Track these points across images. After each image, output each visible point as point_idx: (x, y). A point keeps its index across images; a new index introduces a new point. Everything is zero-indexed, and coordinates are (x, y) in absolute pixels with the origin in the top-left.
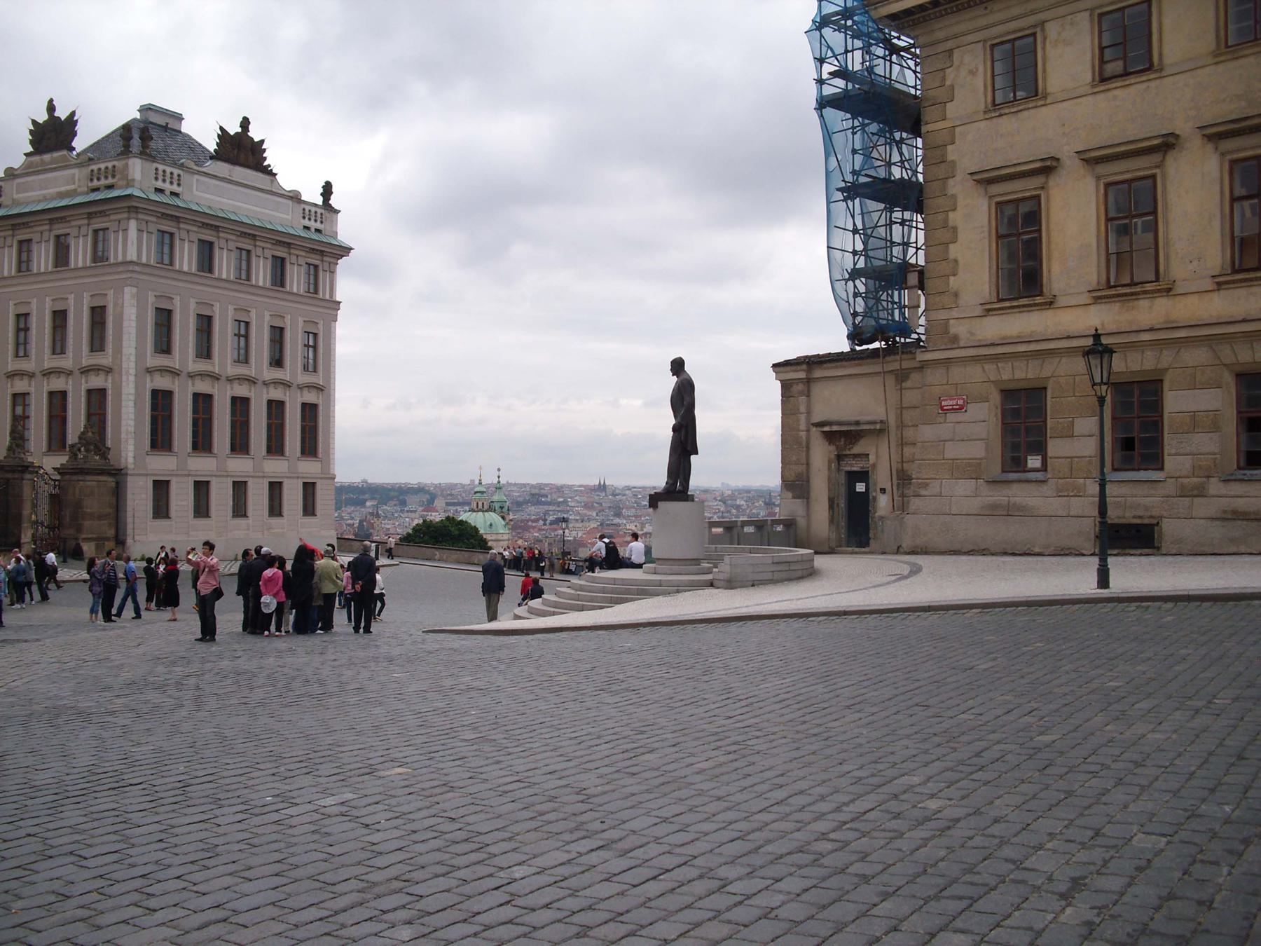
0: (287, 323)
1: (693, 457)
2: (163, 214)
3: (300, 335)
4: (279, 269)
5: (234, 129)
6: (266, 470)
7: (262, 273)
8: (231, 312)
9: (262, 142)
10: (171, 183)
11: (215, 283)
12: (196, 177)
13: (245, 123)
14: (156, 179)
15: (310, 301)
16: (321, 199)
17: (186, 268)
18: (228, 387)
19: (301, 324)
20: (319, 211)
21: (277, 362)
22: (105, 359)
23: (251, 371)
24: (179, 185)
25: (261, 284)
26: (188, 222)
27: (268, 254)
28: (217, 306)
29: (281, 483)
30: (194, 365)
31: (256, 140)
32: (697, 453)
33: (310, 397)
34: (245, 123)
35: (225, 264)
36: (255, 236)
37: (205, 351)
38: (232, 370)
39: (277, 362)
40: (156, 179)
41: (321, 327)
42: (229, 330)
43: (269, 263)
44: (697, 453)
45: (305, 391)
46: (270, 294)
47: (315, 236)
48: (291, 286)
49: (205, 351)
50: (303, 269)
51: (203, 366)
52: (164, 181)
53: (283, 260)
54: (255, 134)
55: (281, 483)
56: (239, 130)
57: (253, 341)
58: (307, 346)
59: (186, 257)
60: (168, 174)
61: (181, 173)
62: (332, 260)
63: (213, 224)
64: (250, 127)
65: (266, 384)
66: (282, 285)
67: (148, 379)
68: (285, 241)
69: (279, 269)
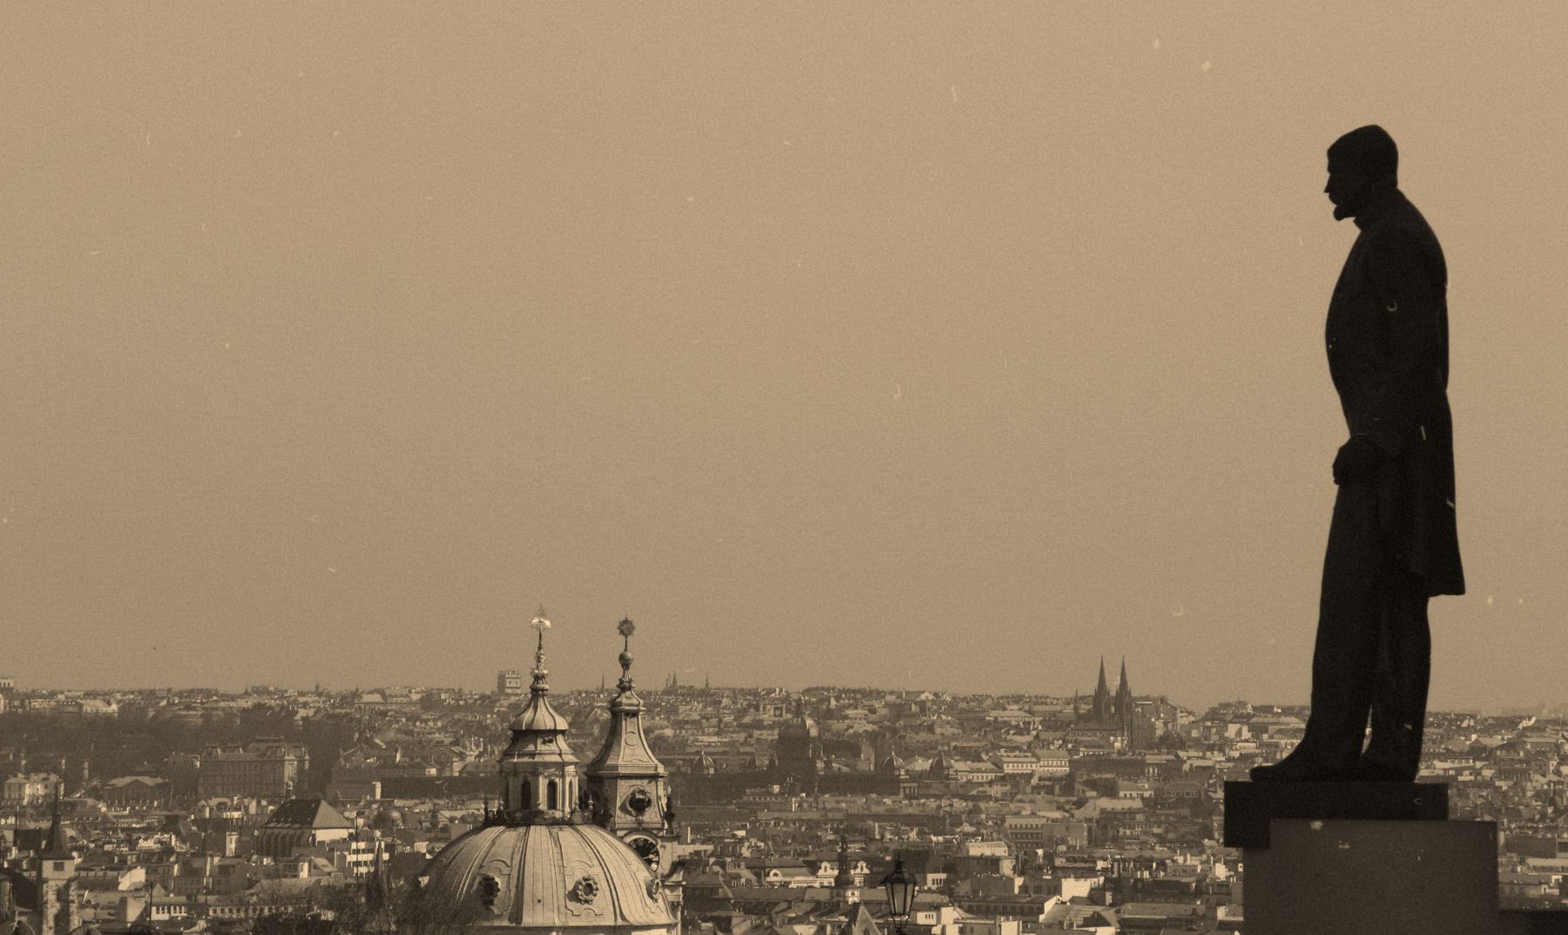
1: (1439, 608)
32: (1455, 585)
44: (1455, 585)
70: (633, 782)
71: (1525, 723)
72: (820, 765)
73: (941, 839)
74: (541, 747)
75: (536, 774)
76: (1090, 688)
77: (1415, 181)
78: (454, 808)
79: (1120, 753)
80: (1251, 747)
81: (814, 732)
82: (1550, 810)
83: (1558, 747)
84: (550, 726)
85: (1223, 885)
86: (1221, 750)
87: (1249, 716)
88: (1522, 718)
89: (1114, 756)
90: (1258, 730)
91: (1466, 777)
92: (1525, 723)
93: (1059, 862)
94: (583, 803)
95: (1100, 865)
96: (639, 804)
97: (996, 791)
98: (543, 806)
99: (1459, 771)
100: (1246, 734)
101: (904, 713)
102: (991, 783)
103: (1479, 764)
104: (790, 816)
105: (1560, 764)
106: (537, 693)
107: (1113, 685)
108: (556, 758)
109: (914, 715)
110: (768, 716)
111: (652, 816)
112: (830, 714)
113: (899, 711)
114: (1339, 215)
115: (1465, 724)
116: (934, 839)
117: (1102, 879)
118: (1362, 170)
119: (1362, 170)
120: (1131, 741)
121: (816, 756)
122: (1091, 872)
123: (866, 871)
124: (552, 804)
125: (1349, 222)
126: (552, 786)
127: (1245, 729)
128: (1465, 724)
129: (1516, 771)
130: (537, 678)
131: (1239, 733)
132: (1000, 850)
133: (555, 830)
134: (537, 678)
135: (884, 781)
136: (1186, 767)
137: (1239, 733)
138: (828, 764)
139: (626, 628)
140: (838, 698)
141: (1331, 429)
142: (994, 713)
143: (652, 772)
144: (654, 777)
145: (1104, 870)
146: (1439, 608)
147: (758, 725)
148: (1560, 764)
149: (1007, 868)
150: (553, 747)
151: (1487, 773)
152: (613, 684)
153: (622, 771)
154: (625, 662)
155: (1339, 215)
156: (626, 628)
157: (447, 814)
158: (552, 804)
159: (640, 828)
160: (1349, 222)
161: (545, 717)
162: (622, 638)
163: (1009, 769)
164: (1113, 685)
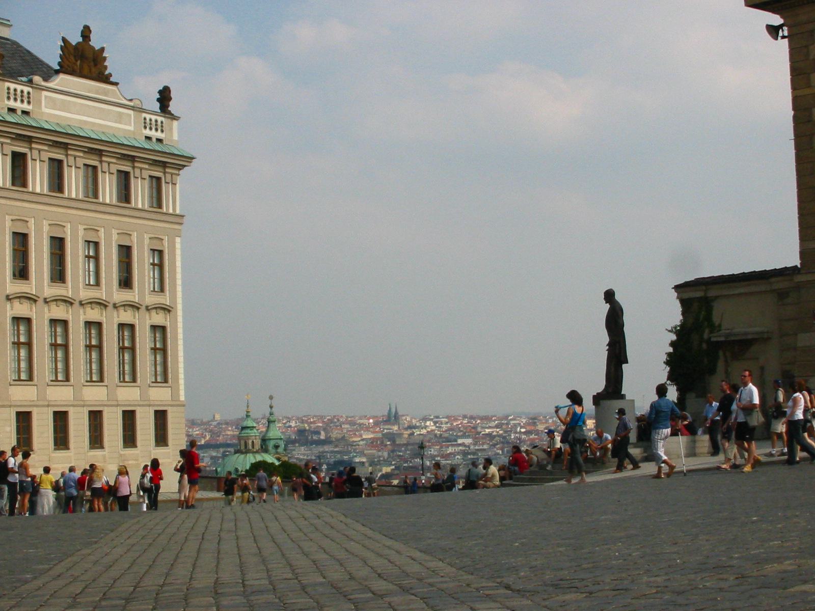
0: (31, 230)
1: (624, 366)
2: (57, 142)
3: (81, 244)
4: (124, 180)
5: (75, 38)
6: (120, 398)
7: (108, 189)
8: (81, 233)
9: (102, 49)
10: (22, 101)
11: (65, 203)
12: (45, 93)
13: (86, 33)
14: (9, 98)
15: (17, 195)
16: (158, 105)
17: (38, 190)
18: (81, 311)
19: (147, 241)
20: (154, 118)
21: (126, 283)
22: (165, 300)
23: (101, 294)
24: (29, 103)
25: (108, 201)
26: (78, 148)
27: (146, 174)
28: (32, 221)
29: (100, 412)
30: (51, 291)
31: (97, 48)
32: (627, 363)
33: (158, 319)
34: (86, 33)
35: (38, 176)
36: (134, 157)
37: (59, 275)
38: (85, 294)
39: (126, 283)
40: (9, 98)
41: (166, 244)
42: (146, 261)
43: (114, 177)
44: (627, 363)
45: (53, 306)
46: (46, 200)
47: (158, 147)
48: (136, 202)
49: (59, 275)
50: (147, 183)
51: (57, 290)
52: (151, 129)
53: (60, 162)
54: (96, 42)
55: (100, 412)
56: (81, 40)
57: (103, 262)
58: (88, 257)
59: (38, 176)
60: (19, 92)
61: (30, 90)
62: (176, 172)
63: (62, 140)
64: (92, 36)
65: (148, 309)
66: (96, 196)
67: (46, 309)
68: (129, 155)
69: (124, 180)
70: (274, 441)
71: (510, 418)
72: (310, 438)
73: (347, 457)
74: (250, 432)
75: (248, 439)
76: (386, 413)
77: (618, 297)
78: (203, 453)
79: (396, 431)
80: (434, 428)
81: (307, 428)
82: (518, 442)
83: (520, 424)
84: (252, 425)
85: (429, 467)
86: (425, 428)
87: (432, 419)
88: (509, 416)
89: (395, 432)
90: (435, 423)
91: (495, 433)
92: (510, 418)
93: (381, 462)
94: (262, 447)
95: (393, 463)
96: (277, 447)
97: (361, 443)
98: (251, 447)
99: (493, 432)
100: (432, 424)
101: (331, 423)
102: (359, 441)
103: (498, 430)
104: (302, 452)
105: (520, 428)
106: (248, 416)
107: (393, 411)
108: (254, 434)
109: (336, 422)
110: (293, 424)
111: (280, 450)
112: (311, 423)
113: (331, 421)
114: (606, 303)
115: (493, 419)
116: (345, 457)
117: (394, 467)
118: (609, 296)
119: (609, 296)
120: (399, 427)
121: (308, 435)
122: (391, 465)
123: (326, 467)
124: (253, 447)
125: (608, 304)
126: (253, 442)
127: (432, 422)
128: (493, 419)
129: (508, 431)
130: (248, 412)
131: (430, 424)
132: (364, 460)
133: (254, 454)
134: (248, 412)
135: (327, 442)
136: (415, 434)
137: (430, 424)
138: (312, 437)
139: (271, 398)
140: (313, 418)
141: (606, 339)
142: (359, 421)
143: (279, 438)
144: (281, 439)
145: (395, 464)
146: (624, 366)
147: (290, 427)
148: (520, 428)
149: (367, 465)
150: (253, 431)
151: (501, 432)
152: (268, 415)
153: (271, 438)
154: (271, 407)
155: (606, 303)
156: (271, 398)
157: (202, 455)
158: (253, 447)
159: (277, 453)
160: (608, 304)
161: (250, 423)
162: (270, 401)
163: (364, 437)
164: (393, 411)
